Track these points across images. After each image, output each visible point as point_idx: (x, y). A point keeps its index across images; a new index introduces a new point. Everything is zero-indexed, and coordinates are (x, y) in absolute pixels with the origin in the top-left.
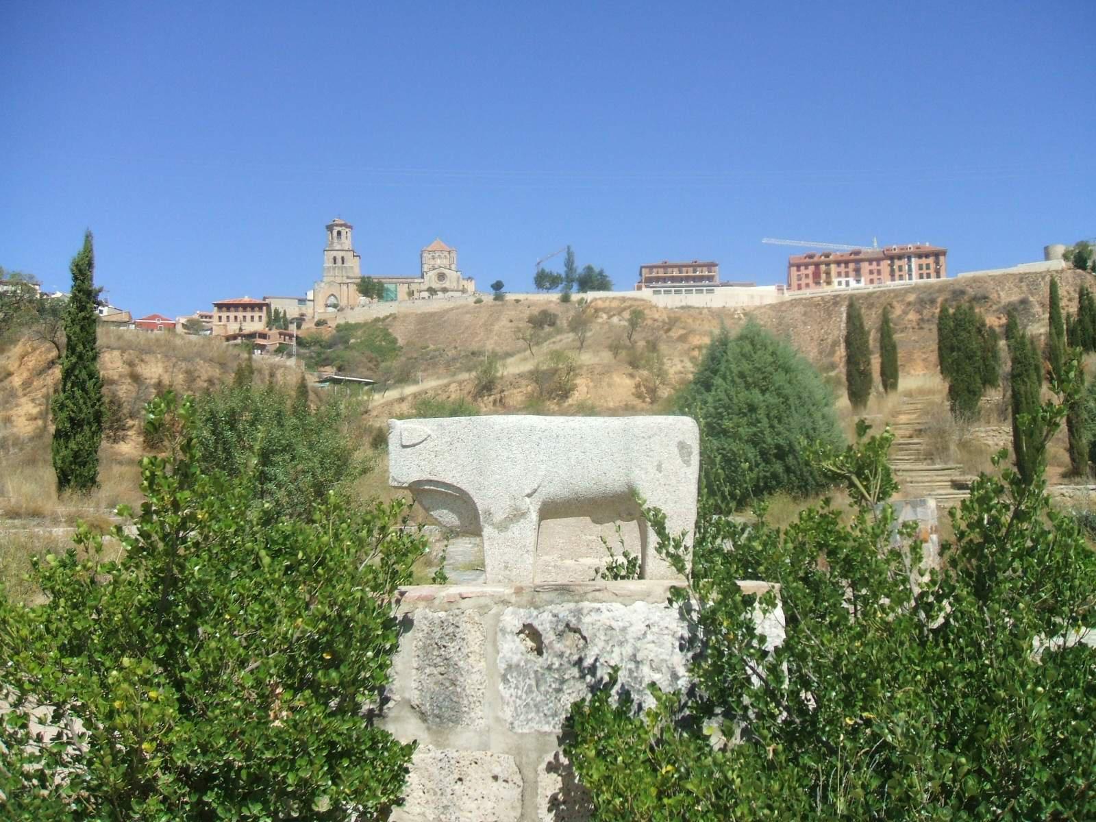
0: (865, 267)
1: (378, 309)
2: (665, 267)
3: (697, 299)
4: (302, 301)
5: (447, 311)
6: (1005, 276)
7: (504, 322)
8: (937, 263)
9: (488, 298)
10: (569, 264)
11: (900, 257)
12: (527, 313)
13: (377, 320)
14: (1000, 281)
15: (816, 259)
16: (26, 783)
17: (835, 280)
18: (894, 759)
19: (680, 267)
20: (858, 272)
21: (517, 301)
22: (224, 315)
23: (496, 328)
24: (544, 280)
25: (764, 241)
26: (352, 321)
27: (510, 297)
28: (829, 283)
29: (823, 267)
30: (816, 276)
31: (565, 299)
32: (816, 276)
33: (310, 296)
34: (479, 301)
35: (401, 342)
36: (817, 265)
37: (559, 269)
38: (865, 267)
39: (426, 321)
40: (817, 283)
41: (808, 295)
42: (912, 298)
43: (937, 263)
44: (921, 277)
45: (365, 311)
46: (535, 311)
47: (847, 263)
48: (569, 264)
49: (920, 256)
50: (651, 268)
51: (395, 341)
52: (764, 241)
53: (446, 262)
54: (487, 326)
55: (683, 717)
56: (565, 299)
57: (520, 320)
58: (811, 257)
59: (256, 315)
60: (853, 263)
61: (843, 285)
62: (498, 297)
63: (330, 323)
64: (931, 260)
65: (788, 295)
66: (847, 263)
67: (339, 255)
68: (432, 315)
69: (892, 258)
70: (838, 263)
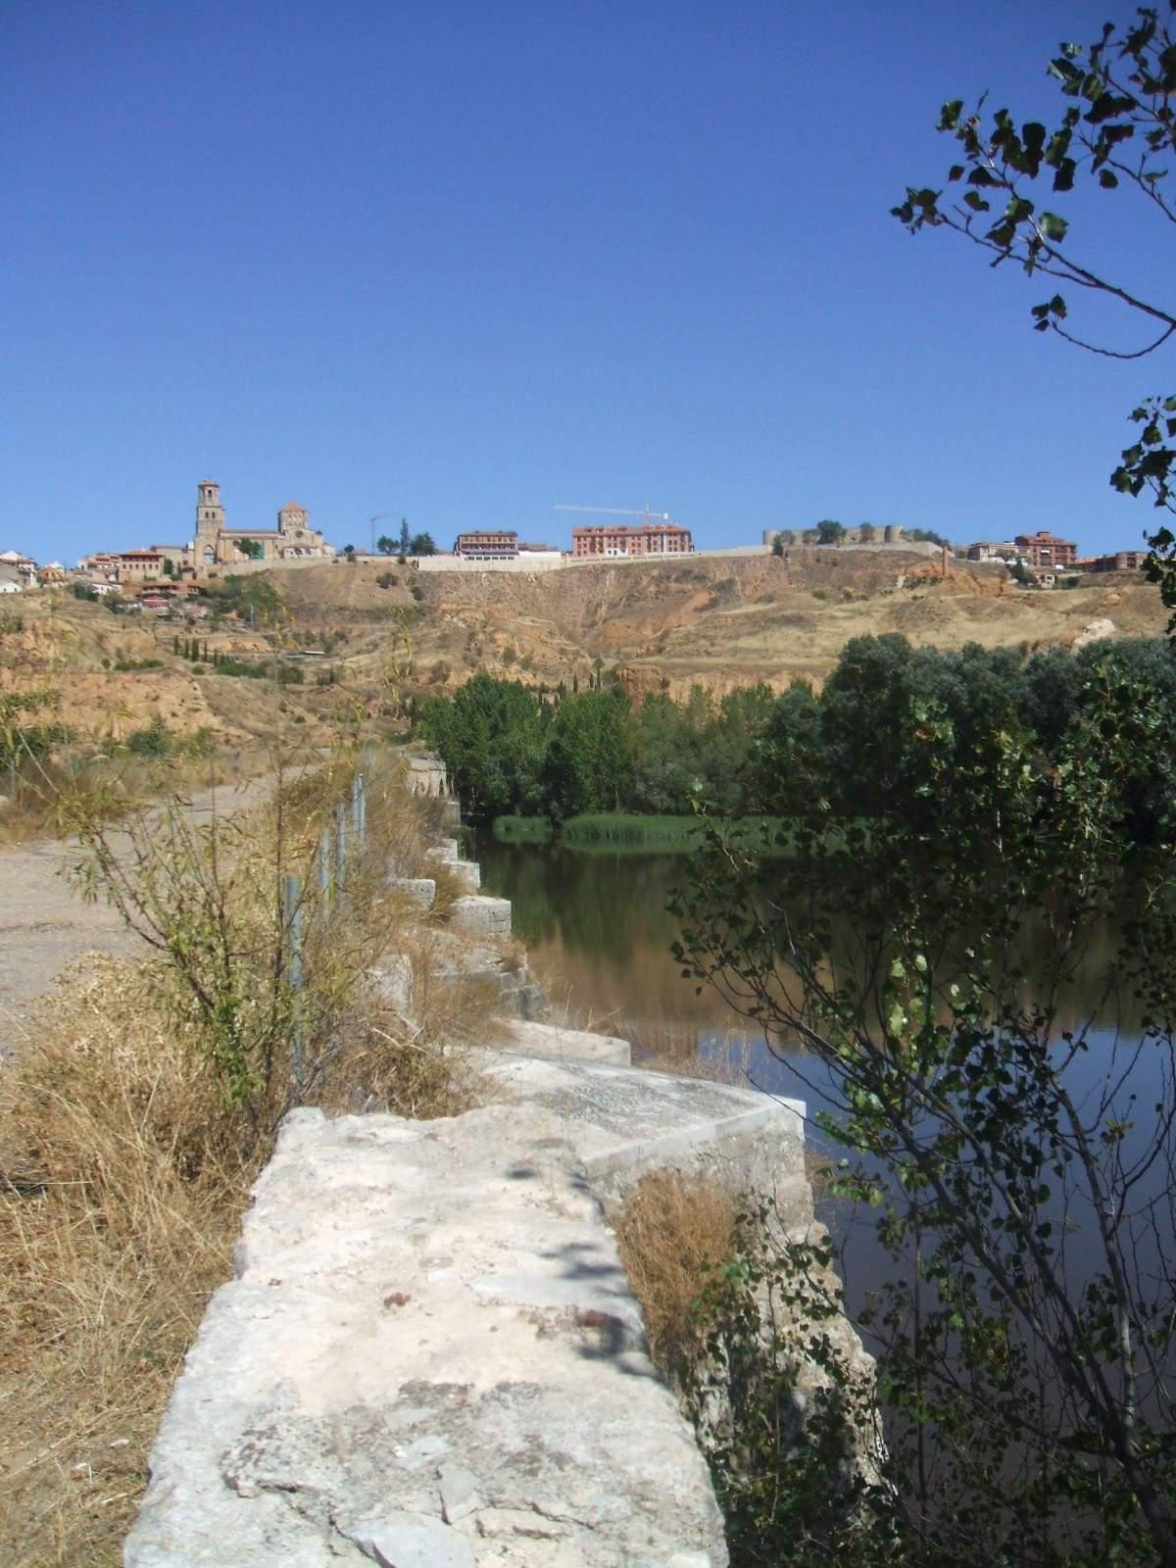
0: (629, 540)
1: (257, 566)
2: (477, 536)
3: (500, 565)
4: (185, 550)
6: (724, 559)
7: (358, 581)
8: (682, 540)
9: (343, 560)
10: (404, 532)
11: (655, 535)
12: (375, 575)
13: (257, 574)
14: (717, 561)
17: (606, 550)
19: (488, 537)
20: (623, 544)
22: (128, 564)
23: (353, 586)
24: (385, 545)
25: (557, 507)
26: (236, 574)
27: (360, 559)
28: (601, 551)
31: (402, 562)
33: (191, 546)
34: (336, 562)
36: (593, 538)
37: (397, 537)
38: (629, 540)
39: (297, 575)
40: (593, 550)
41: (585, 563)
42: (655, 573)
43: (682, 540)
45: (242, 565)
46: (382, 574)
48: (404, 532)
49: (670, 534)
50: (466, 536)
52: (557, 507)
53: (300, 520)
54: (347, 584)
55: (1026, 142)
56: (402, 562)
57: (370, 580)
59: (154, 564)
60: (620, 537)
61: (614, 555)
62: (351, 559)
63: (219, 575)
64: (678, 538)
65: (570, 562)
67: (210, 510)
69: (649, 535)
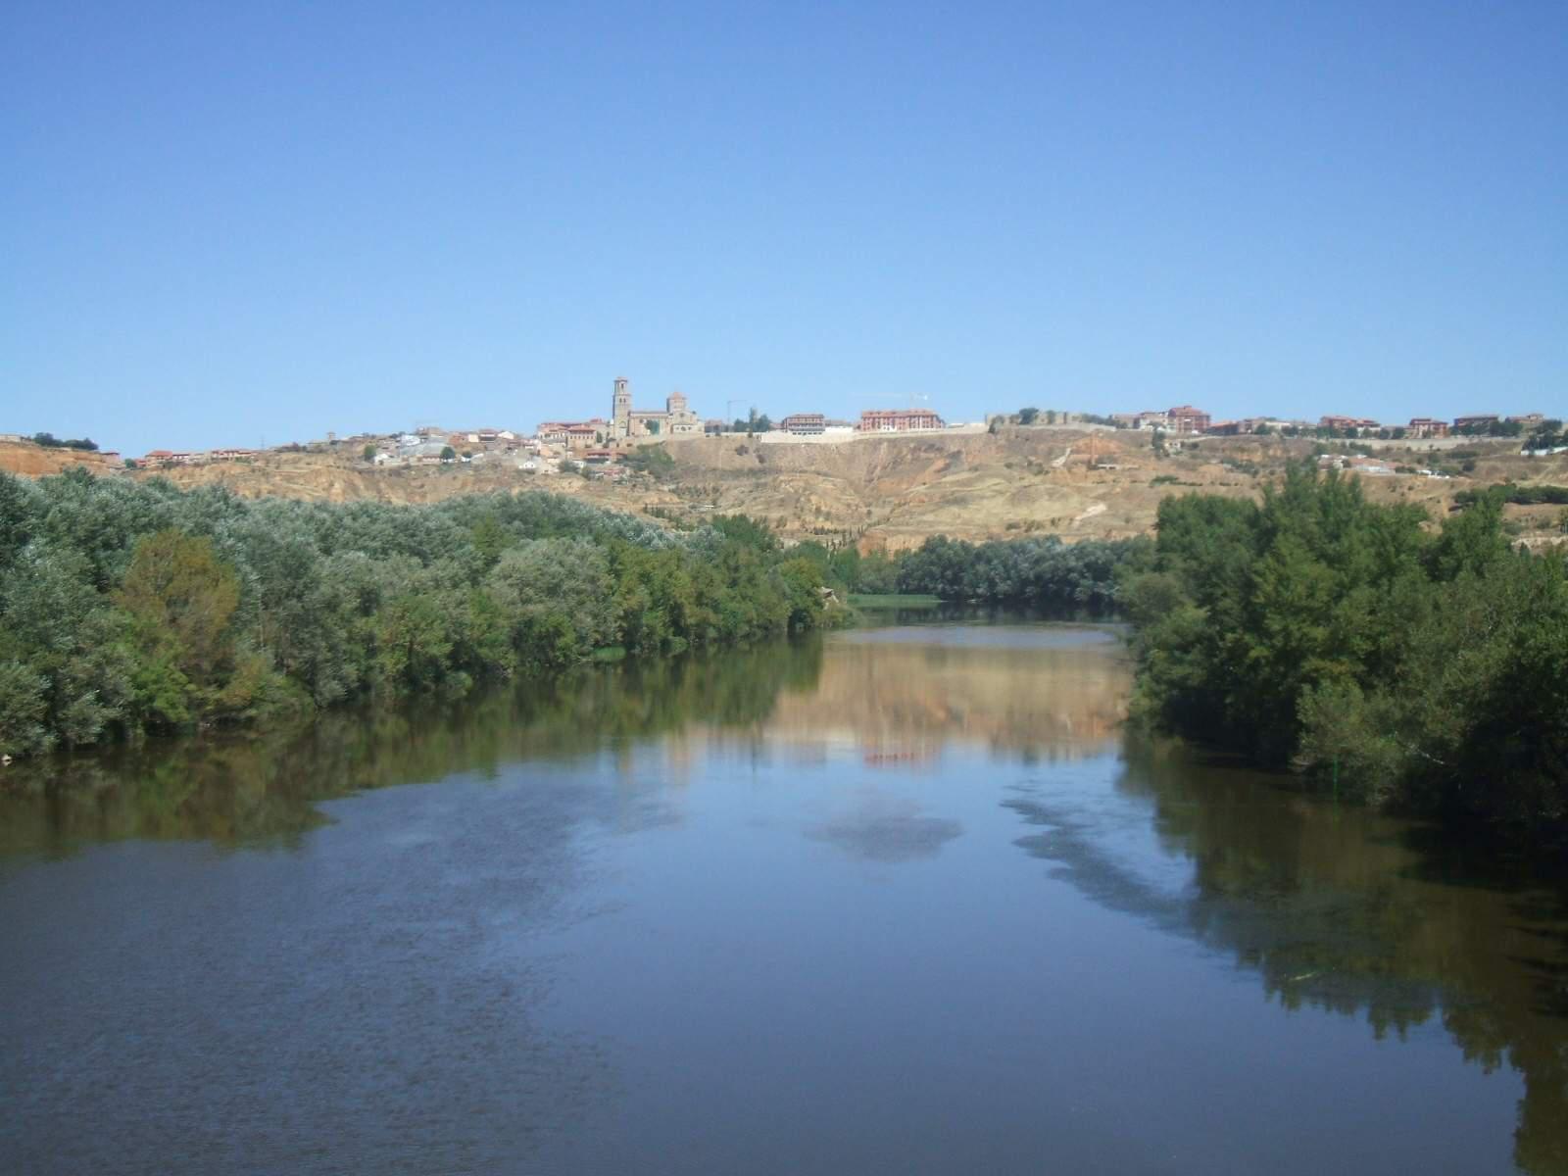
3: (812, 438)
5: (694, 440)
8: (932, 420)
11: (915, 417)
15: (874, 416)
16: (1430, 621)
17: (883, 427)
18: (1432, 660)
21: (727, 437)
22: (574, 436)
26: (644, 443)
29: (877, 420)
30: (873, 426)
32: (873, 426)
35: (674, 458)
37: (746, 419)
38: (897, 421)
43: (932, 420)
44: (924, 427)
47: (888, 418)
49: (923, 417)
51: (669, 458)
56: (750, 436)
58: (871, 413)
64: (929, 419)
66: (888, 418)
68: (685, 442)
69: (911, 417)
70: (884, 418)
